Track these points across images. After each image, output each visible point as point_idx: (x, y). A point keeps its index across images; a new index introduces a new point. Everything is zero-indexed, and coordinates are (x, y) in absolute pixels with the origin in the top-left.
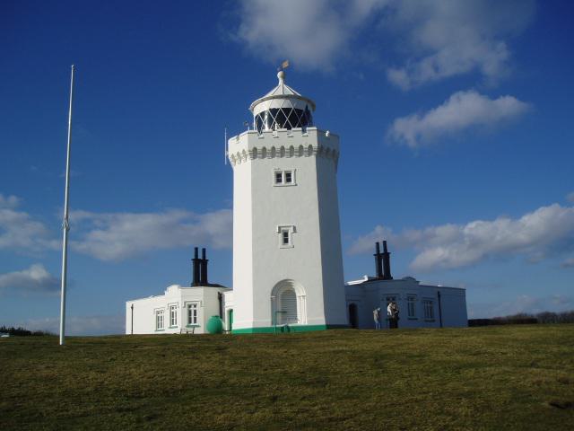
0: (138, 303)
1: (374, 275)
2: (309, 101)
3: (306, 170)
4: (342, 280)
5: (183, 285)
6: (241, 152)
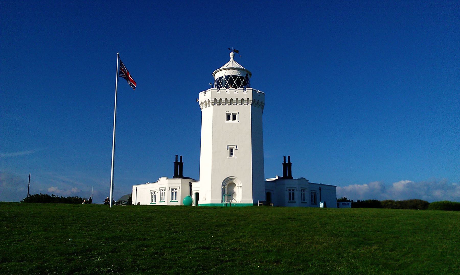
0: (140, 187)
1: (282, 176)
2: (248, 72)
3: (245, 113)
4: (263, 178)
5: (168, 177)
6: (207, 100)
